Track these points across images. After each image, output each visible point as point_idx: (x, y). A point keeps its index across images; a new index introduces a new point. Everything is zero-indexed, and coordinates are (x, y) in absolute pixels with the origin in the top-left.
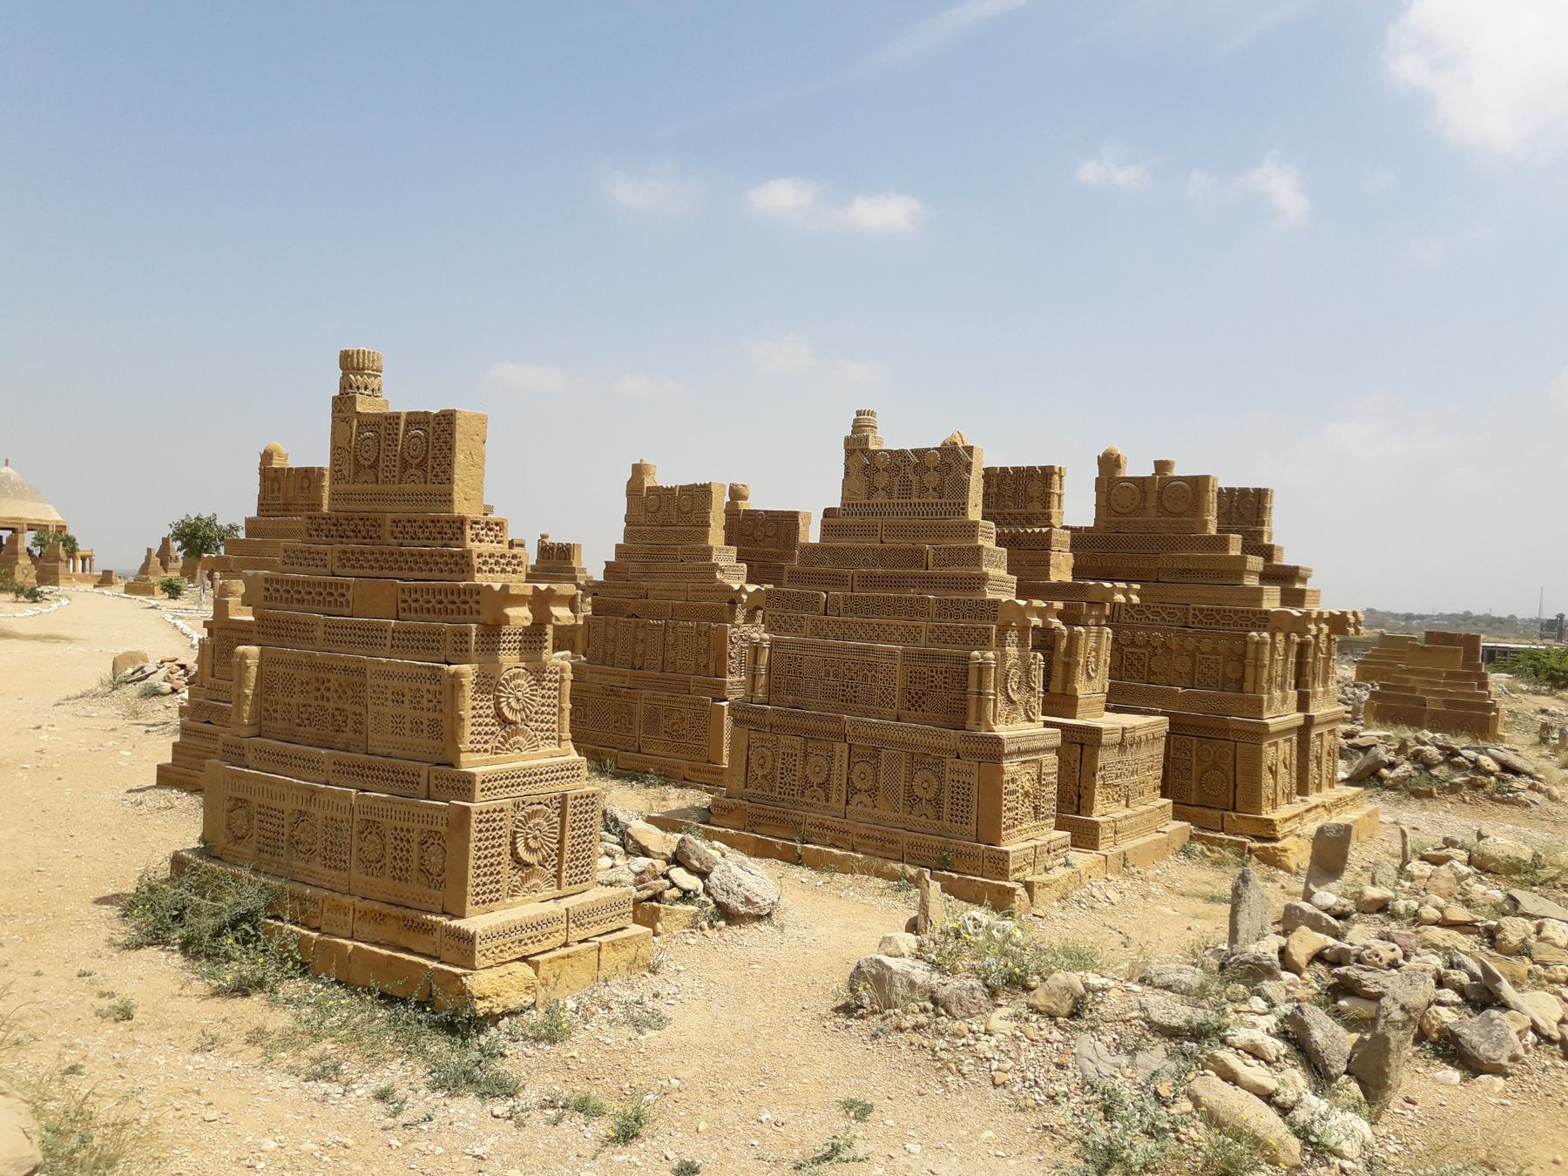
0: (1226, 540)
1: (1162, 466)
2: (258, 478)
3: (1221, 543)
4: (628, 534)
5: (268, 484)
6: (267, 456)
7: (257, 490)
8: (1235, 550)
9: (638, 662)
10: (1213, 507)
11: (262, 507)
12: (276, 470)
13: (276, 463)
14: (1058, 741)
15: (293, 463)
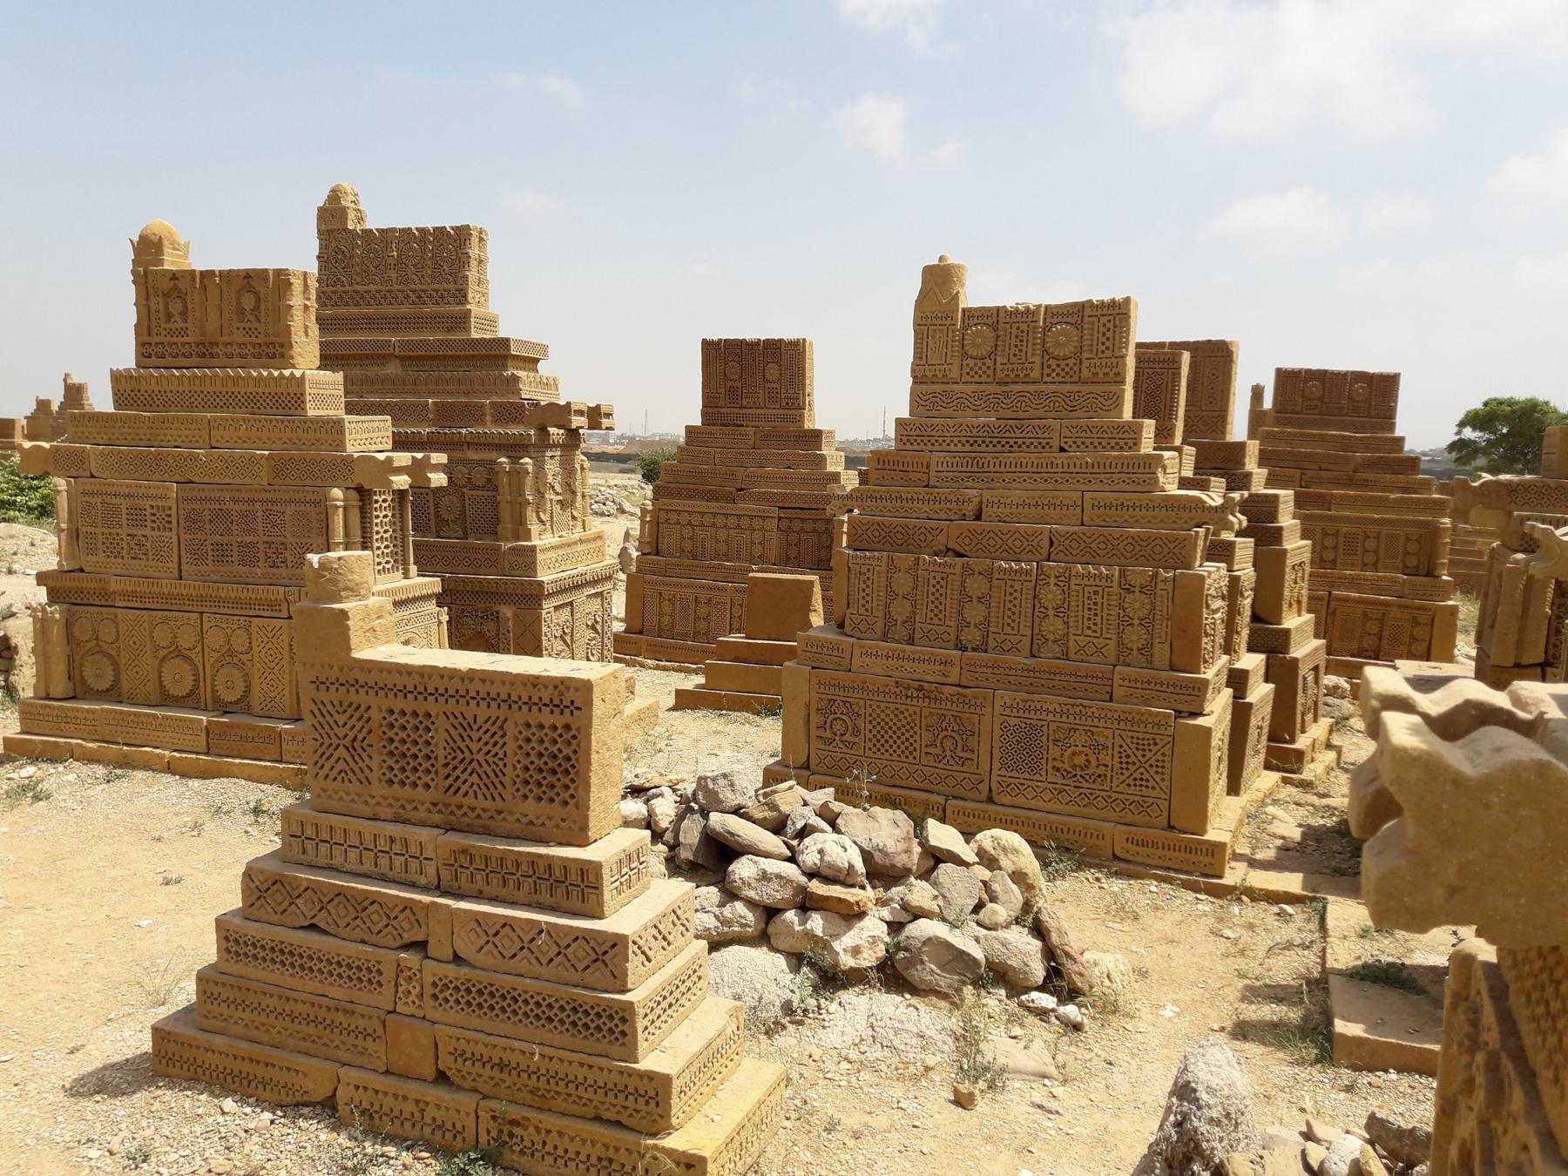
0: (1141, 426)
1: (941, 259)
2: (129, 292)
3: (1133, 433)
4: (916, 400)
5: (157, 303)
6: (148, 249)
7: (131, 316)
8: (1147, 446)
9: (972, 636)
10: (1131, 362)
11: (147, 348)
12: (174, 276)
13: (171, 262)
14: (438, 589)
15: (199, 261)
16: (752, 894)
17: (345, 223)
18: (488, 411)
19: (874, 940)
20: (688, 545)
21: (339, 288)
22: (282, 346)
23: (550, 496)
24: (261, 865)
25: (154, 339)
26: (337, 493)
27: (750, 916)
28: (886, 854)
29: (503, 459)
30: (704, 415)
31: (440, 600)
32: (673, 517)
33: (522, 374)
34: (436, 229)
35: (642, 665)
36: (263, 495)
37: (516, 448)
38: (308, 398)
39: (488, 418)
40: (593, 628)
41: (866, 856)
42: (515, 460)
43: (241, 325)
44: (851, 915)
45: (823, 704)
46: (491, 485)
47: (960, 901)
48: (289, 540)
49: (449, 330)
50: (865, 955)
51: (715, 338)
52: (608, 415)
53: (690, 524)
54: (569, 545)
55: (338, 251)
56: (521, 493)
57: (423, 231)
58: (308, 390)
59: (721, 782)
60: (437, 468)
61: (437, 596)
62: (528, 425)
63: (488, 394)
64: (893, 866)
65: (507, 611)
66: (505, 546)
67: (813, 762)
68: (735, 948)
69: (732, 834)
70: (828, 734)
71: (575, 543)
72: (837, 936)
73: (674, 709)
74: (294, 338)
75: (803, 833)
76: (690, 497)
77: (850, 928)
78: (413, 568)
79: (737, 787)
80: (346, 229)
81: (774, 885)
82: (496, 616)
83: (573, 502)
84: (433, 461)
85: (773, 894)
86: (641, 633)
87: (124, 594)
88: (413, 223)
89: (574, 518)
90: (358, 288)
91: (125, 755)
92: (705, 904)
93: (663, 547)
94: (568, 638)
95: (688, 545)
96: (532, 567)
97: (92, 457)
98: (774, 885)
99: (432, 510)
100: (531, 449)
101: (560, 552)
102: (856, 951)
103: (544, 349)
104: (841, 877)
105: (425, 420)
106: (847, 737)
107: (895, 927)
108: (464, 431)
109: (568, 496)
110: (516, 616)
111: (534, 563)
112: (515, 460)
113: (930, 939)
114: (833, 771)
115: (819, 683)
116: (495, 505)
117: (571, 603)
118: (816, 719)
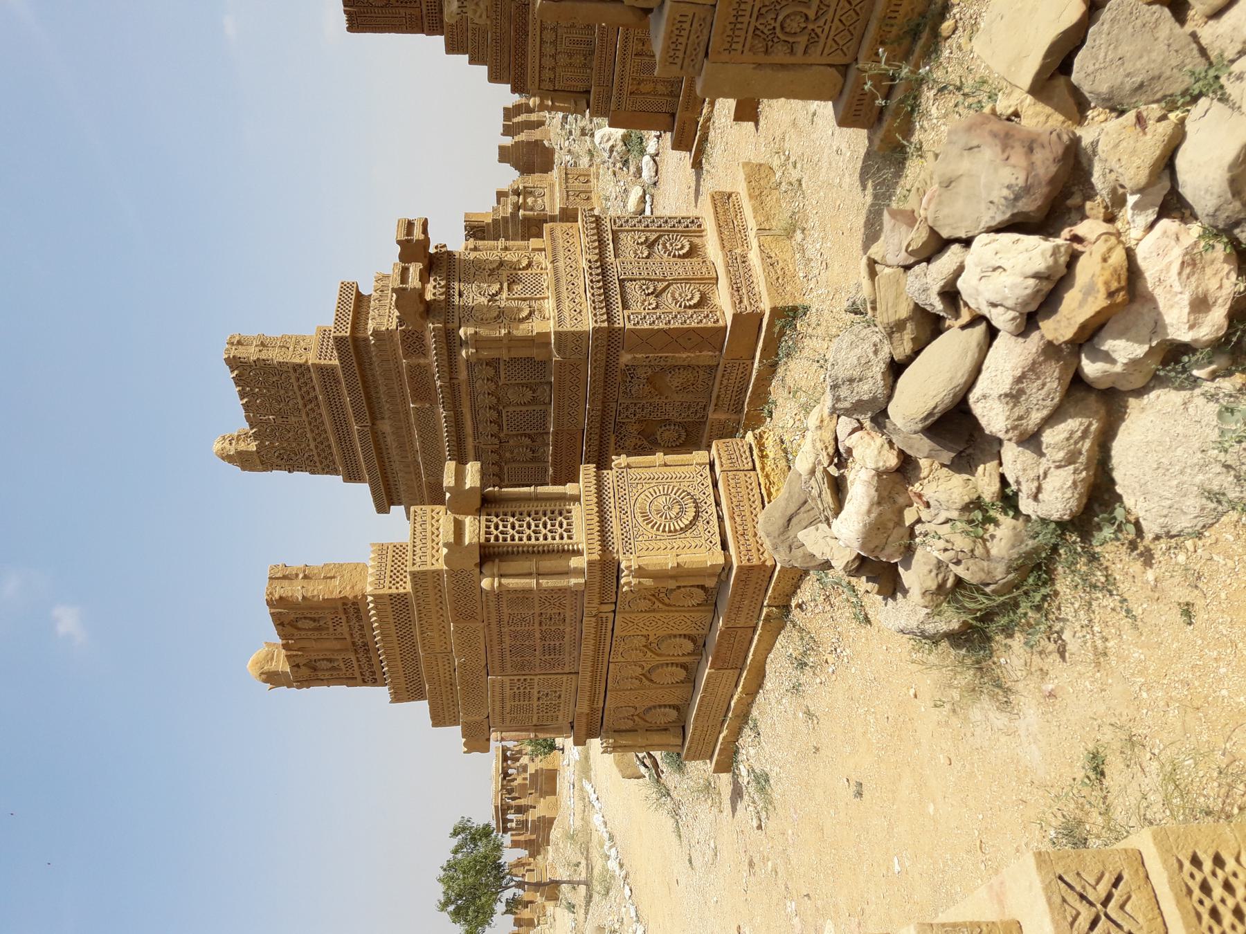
2: (315, 690)
16: (1036, 417)
17: (252, 452)
18: (414, 361)
19: (1191, 263)
20: (578, 60)
21: (316, 458)
22: (344, 604)
23: (503, 300)
24: (841, 113)
25: (357, 674)
26: (485, 583)
27: (1073, 424)
28: (1028, 189)
29: (464, 353)
30: (431, 32)
31: (602, 464)
32: (547, 74)
33: (371, 326)
34: (237, 384)
35: (709, 119)
36: (494, 626)
37: (450, 341)
38: (394, 591)
39: (422, 361)
40: (651, 245)
41: (1017, 225)
42: (463, 343)
43: (331, 630)
44: (1131, 283)
45: (760, 46)
46: (493, 363)
47: (1158, 52)
48: (537, 610)
49: (337, 382)
50: (1213, 285)
51: (344, 17)
52: (410, 225)
53: (554, 57)
54: (557, 280)
55: (280, 457)
56: (500, 340)
57: (242, 395)
58: (386, 591)
59: (844, 392)
60: (460, 476)
61: (599, 468)
62: (424, 328)
63: (398, 366)
64: (1052, 181)
65: (625, 358)
66: (556, 357)
67: (839, 59)
68: (1119, 448)
69: (930, 414)
70: (803, 40)
71: (556, 269)
72: (1158, 325)
73: (757, 124)
74: (335, 595)
75: (951, 295)
76: (524, 54)
77: (1150, 299)
78: (570, 489)
79: (856, 374)
80: (258, 452)
81: (1032, 388)
82: (630, 369)
83: (514, 267)
84: (452, 484)
85: (1049, 387)
86: (673, 115)
87: (592, 701)
88: (238, 404)
89: (529, 265)
90: (312, 446)
91: (736, 716)
92: (1032, 475)
93: (581, 86)
94: (661, 286)
95: (578, 60)
96: (578, 336)
97: (470, 719)
98: (1032, 388)
99: (524, 409)
100: (450, 326)
101: (565, 294)
102: (1200, 305)
103: (345, 287)
104: (1051, 290)
105: (433, 410)
106: (812, 15)
107: (1173, 205)
108: (438, 383)
109: (504, 273)
110: (630, 351)
111: (573, 333)
112: (463, 343)
113: (1233, 182)
114: (857, 33)
115: (729, 50)
116: (513, 360)
117: (621, 281)
118: (780, 55)
